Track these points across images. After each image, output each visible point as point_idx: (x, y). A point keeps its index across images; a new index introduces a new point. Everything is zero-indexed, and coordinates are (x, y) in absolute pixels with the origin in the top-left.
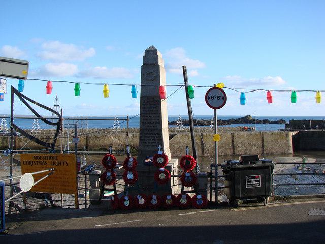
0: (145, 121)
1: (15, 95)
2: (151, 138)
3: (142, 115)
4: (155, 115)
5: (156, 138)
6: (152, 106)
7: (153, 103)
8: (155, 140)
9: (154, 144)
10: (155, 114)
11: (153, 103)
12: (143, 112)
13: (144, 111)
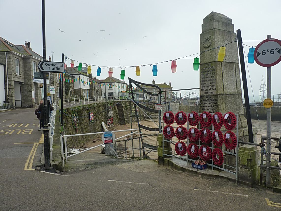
4: (211, 82)
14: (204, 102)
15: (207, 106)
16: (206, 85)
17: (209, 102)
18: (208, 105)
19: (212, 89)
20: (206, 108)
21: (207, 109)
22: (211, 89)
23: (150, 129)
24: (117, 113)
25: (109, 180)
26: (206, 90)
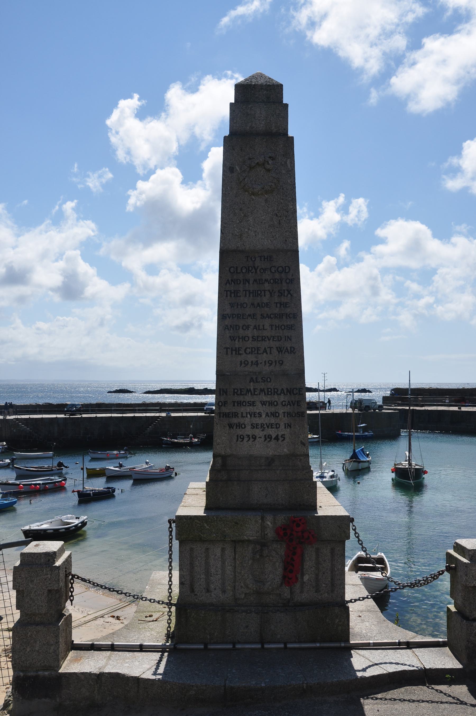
0: (237, 344)
1: (162, 613)
2: (259, 408)
3: (228, 322)
4: (276, 322)
5: (281, 410)
6: (267, 286)
7: (267, 276)
8: (275, 415)
9: (273, 432)
10: (280, 316)
11: (267, 276)
12: (228, 311)
13: (232, 305)
14: (241, 398)
15: (253, 415)
16: (249, 333)
17: (265, 398)
18: (258, 411)
19: (280, 350)
20: (247, 421)
21: (254, 426)
22: (275, 351)
23: (4, 467)
24: (20, 388)
25: (465, 561)
26: (251, 353)
